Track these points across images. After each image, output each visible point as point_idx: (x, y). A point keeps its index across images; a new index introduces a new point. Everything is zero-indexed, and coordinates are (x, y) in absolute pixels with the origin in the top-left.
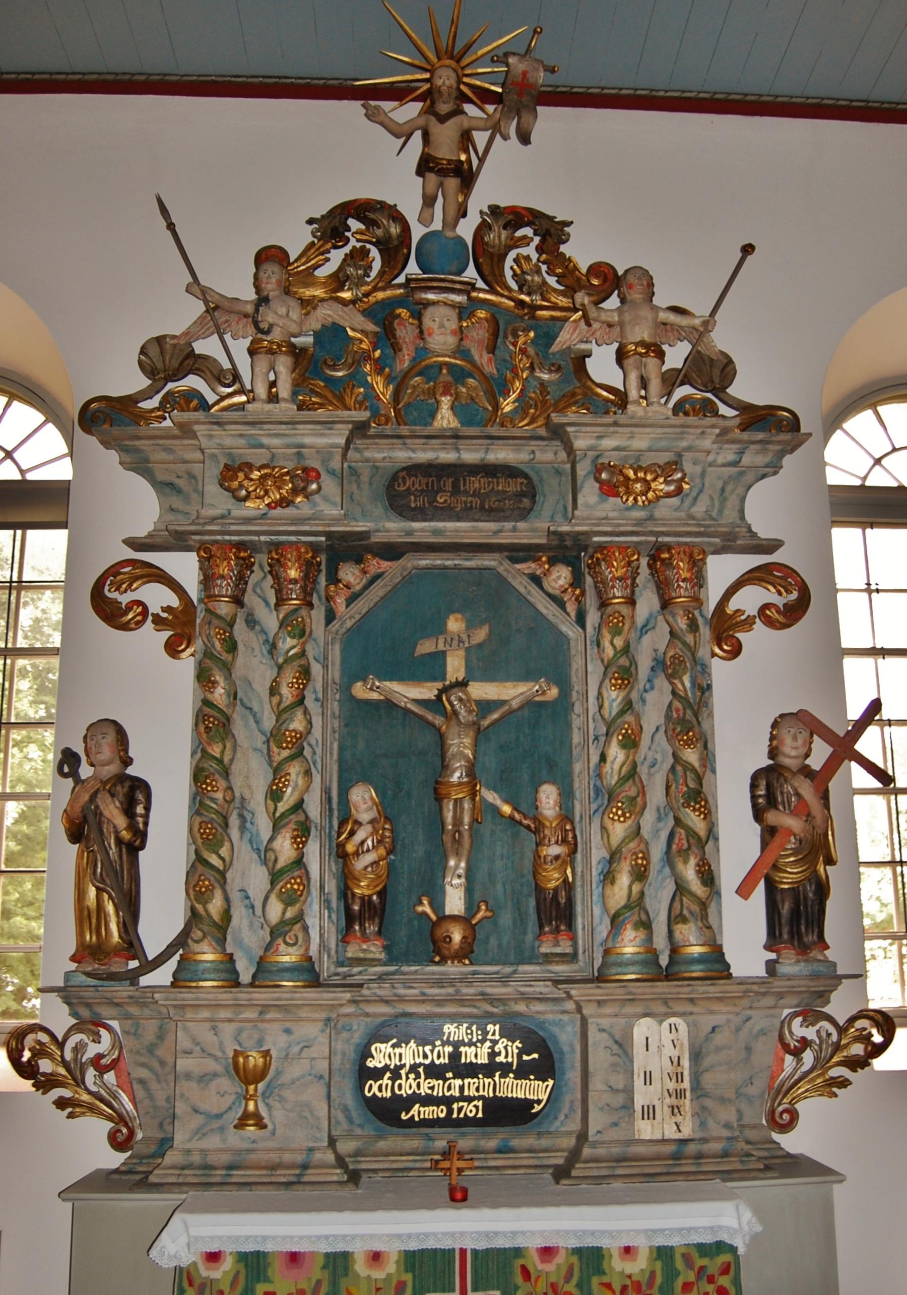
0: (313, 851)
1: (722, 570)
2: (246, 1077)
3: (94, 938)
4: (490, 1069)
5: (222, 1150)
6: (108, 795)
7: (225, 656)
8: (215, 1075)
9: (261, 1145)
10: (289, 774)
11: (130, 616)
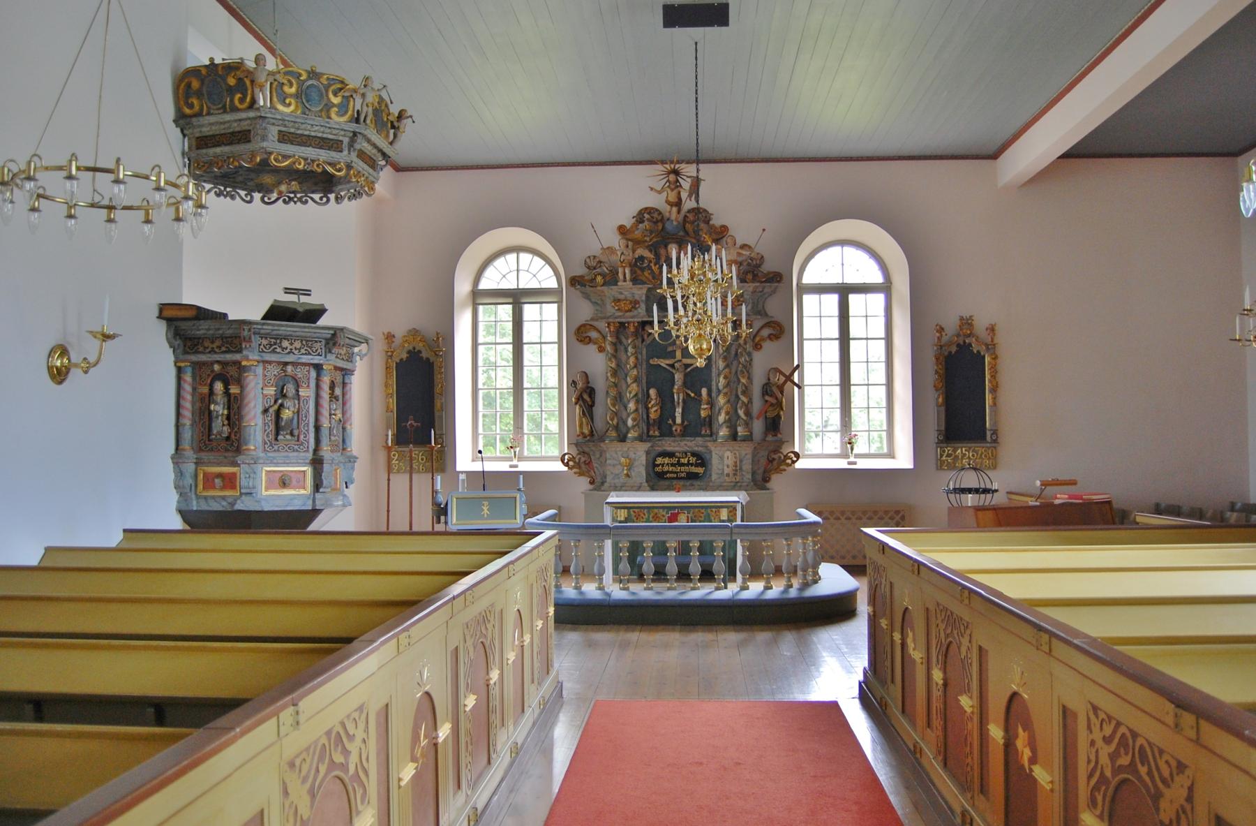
4: (688, 464)
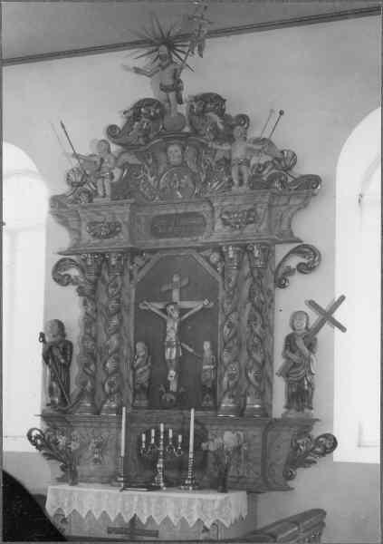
1: (281, 251)
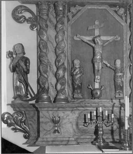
0: (66, 74)
2: (55, 123)
3: (19, 93)
5: (50, 138)
6: (21, 61)
7: (46, 29)
8: (48, 122)
9: (59, 136)
10: (61, 56)
11: (22, 19)
